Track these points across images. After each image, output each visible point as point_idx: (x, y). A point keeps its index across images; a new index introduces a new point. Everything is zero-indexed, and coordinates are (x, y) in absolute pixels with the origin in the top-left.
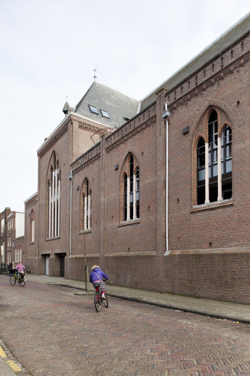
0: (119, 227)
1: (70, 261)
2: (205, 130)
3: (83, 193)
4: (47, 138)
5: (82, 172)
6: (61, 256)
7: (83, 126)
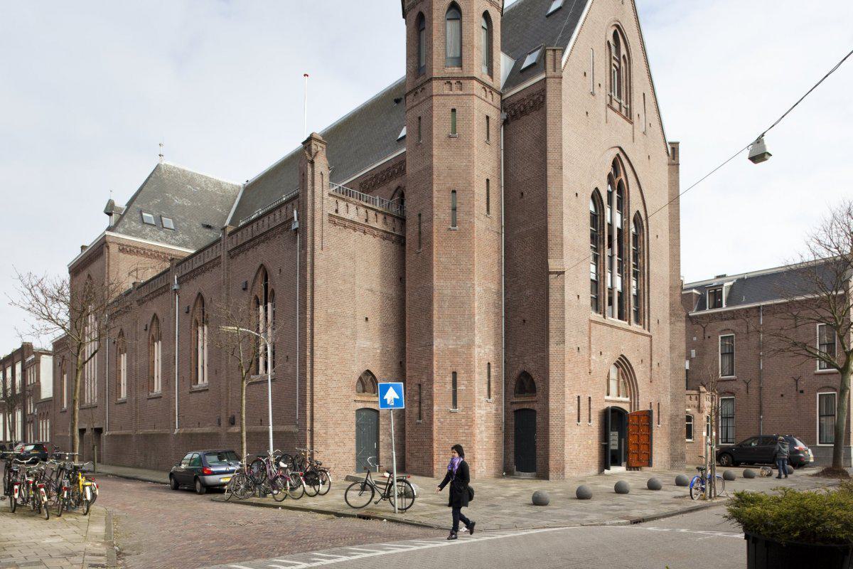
0: (148, 399)
1: (106, 440)
2: (448, 211)
3: (256, 298)
4: (87, 245)
5: (192, 282)
6: (99, 431)
7: (125, 249)
